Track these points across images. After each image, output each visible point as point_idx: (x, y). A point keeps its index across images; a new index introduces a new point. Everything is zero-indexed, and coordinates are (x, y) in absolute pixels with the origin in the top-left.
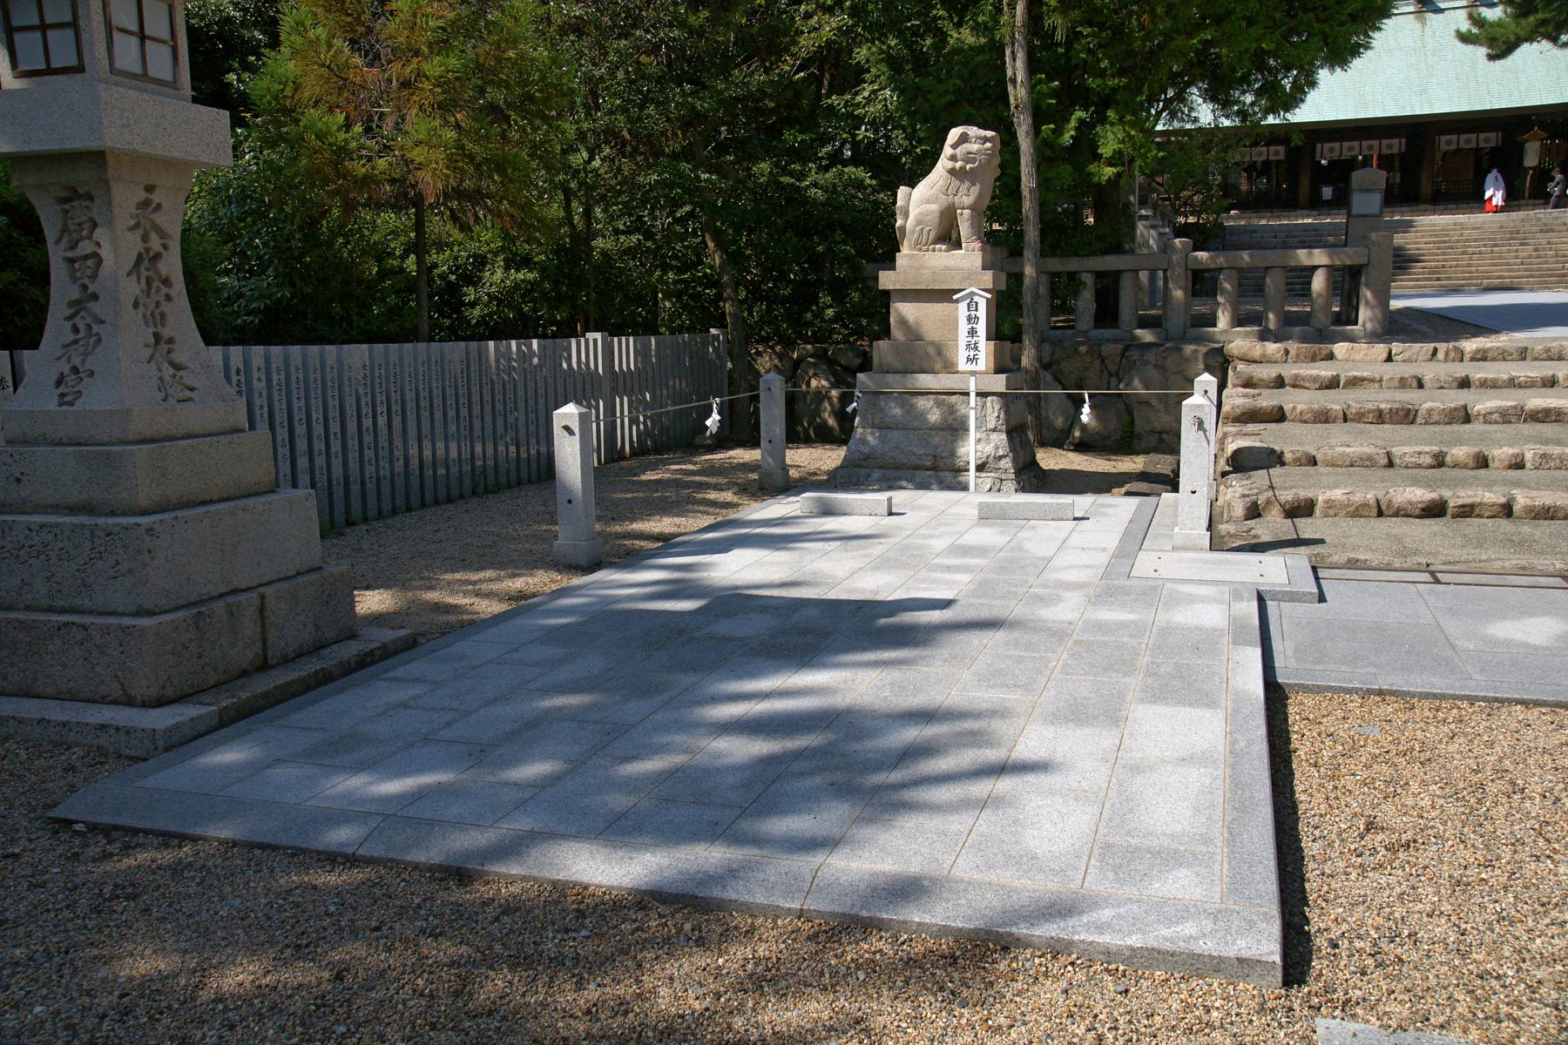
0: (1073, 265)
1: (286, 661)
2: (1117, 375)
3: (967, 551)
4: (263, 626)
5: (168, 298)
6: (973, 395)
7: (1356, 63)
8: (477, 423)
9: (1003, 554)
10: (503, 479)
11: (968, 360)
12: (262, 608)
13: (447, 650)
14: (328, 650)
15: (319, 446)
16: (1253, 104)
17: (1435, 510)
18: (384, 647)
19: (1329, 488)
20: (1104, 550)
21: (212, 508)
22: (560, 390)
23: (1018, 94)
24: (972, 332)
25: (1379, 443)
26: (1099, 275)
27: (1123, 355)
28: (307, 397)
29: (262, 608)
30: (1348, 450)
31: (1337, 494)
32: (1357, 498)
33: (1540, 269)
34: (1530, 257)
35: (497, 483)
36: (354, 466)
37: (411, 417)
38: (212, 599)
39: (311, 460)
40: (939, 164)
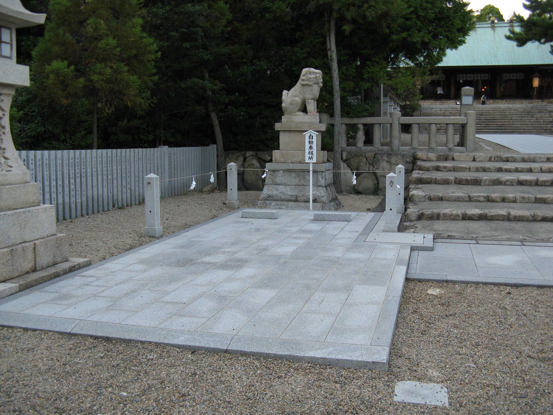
0: (355, 121)
1: (43, 269)
2: (372, 165)
3: (304, 232)
4: (35, 255)
5: (4, 133)
6: (311, 172)
7: (460, 48)
8: (115, 181)
9: (318, 233)
10: (125, 204)
11: (309, 158)
12: (35, 249)
13: (102, 266)
14: (58, 265)
15: (54, 189)
16: (423, 61)
17: (482, 218)
18: (79, 264)
19: (445, 209)
20: (357, 232)
21: (18, 211)
22: (148, 168)
23: (333, 54)
24: (311, 148)
25: (466, 192)
26: (365, 125)
27: (374, 157)
28: (50, 170)
29: (35, 249)
30: (454, 194)
31: (447, 211)
32: (455, 212)
33: (538, 127)
34: (534, 122)
35: (123, 205)
36: (67, 200)
37: (89, 179)
38: (17, 244)
39: (51, 195)
40: (299, 82)
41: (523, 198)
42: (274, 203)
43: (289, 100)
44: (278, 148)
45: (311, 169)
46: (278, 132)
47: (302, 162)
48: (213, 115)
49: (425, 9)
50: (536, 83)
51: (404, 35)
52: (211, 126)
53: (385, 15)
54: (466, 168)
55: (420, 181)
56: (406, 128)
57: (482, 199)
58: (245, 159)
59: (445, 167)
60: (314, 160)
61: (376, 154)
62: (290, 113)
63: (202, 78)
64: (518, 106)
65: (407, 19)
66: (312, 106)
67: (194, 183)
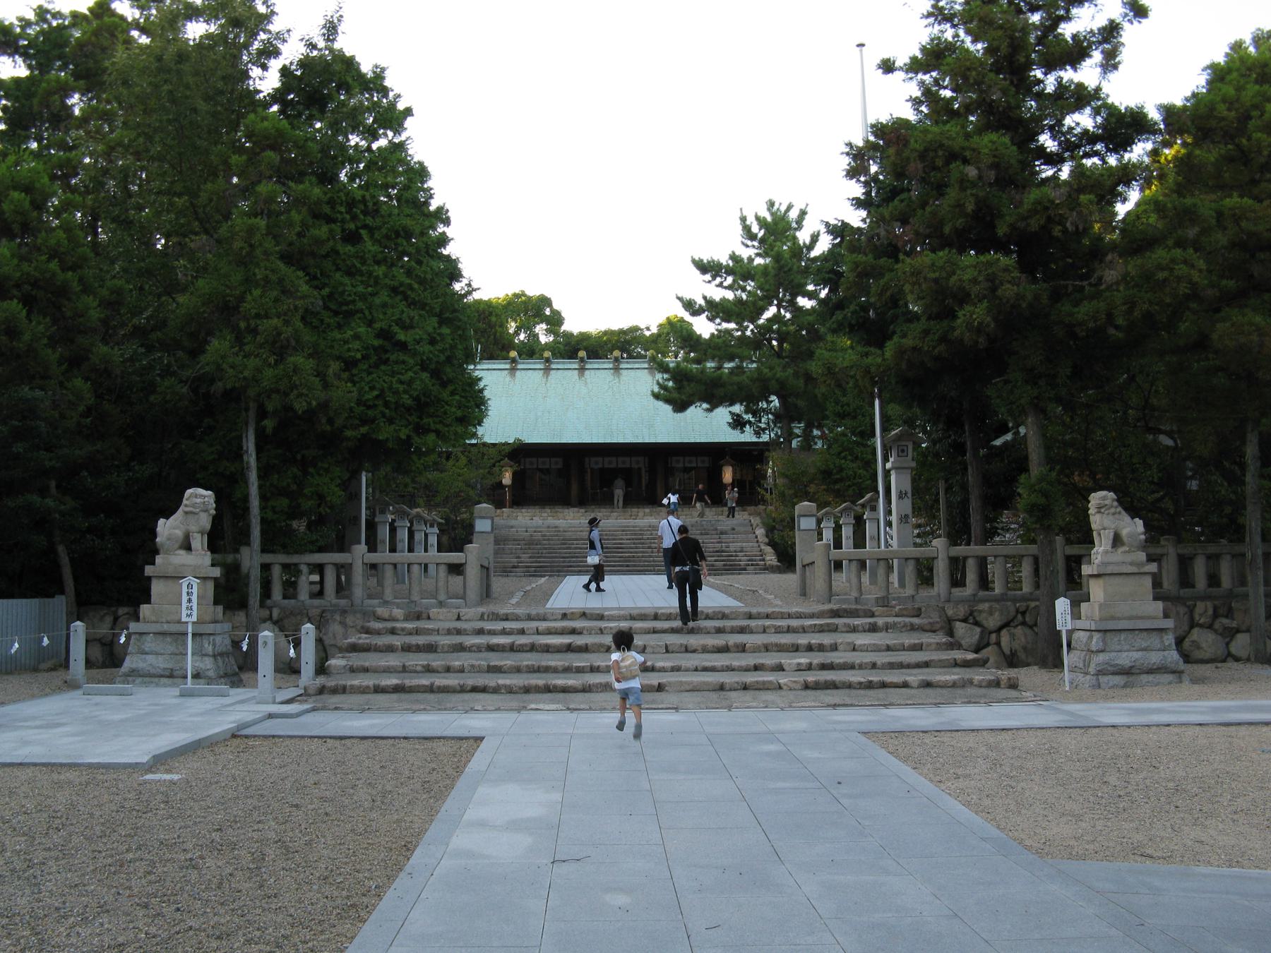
0: (294, 559)
6: (190, 636)
24: (190, 601)
41: (473, 666)
42: (139, 680)
43: (166, 533)
44: (148, 601)
45: (190, 630)
46: (149, 579)
47: (179, 622)
48: (61, 549)
49: (396, 392)
50: (728, 475)
51: (364, 430)
52: (57, 566)
53: (324, 406)
54: (433, 630)
57: (419, 668)
58: (116, 619)
59: (403, 629)
60: (194, 619)
61: (323, 612)
62: (167, 552)
63: (43, 492)
65: (369, 407)
66: (199, 542)
67: (17, 645)
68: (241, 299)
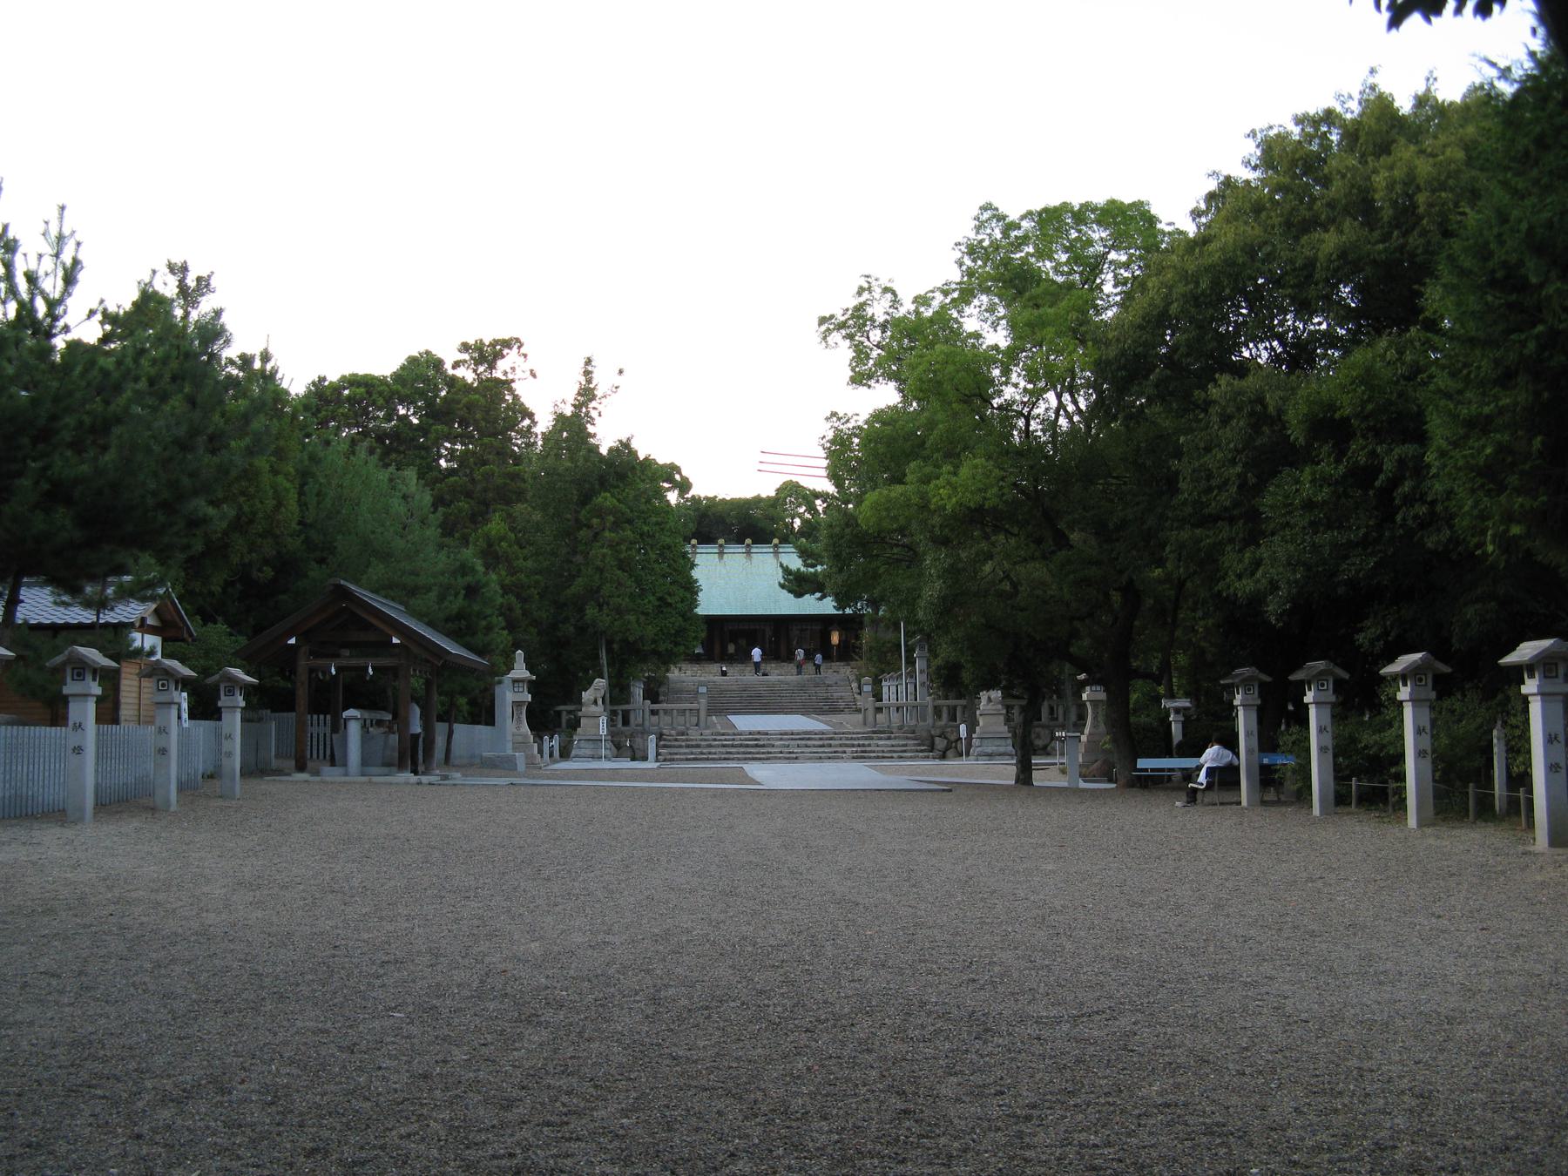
46: (66, 697)
50: (835, 638)
53: (641, 638)
55: (665, 746)
56: (654, 713)
64: (781, 675)
66: (600, 701)
68: (599, 588)
